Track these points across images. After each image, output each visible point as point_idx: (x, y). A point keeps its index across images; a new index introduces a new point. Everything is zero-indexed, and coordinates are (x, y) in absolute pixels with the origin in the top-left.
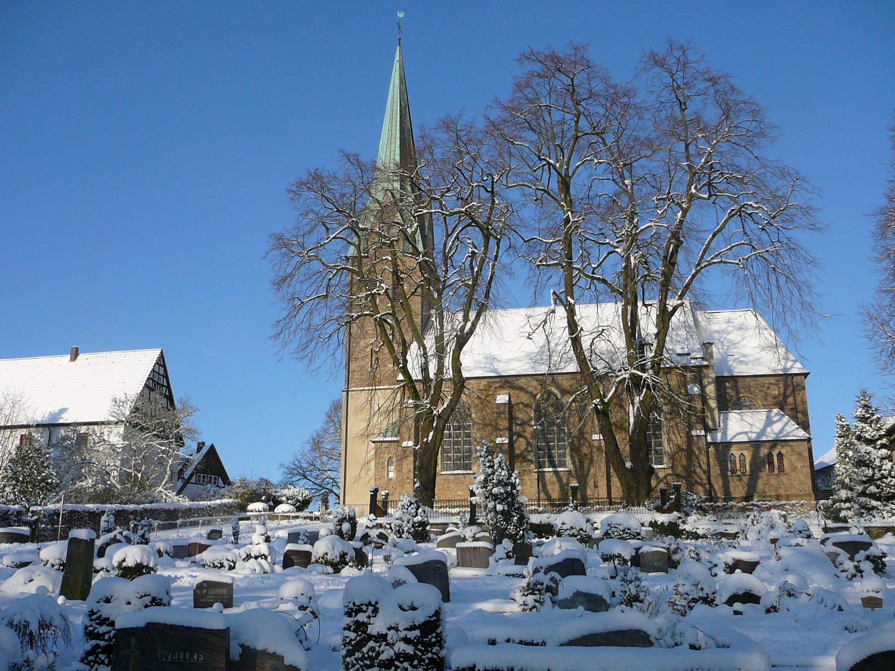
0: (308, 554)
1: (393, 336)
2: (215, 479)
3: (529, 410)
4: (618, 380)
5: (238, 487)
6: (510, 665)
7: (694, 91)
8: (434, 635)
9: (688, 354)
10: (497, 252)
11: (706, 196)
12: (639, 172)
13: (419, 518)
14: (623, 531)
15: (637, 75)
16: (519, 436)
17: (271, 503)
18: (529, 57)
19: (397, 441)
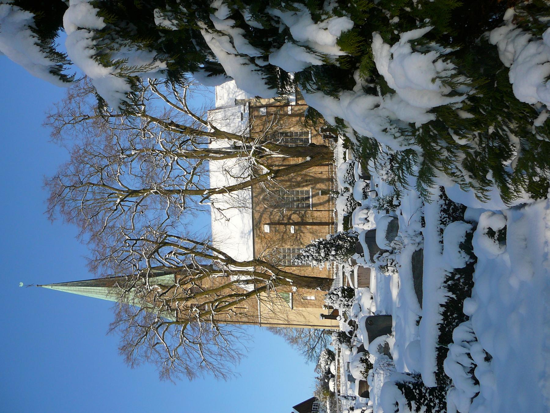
0: (361, 382)
1: (226, 301)
2: (314, 406)
3: (274, 213)
4: (256, 164)
5: (319, 396)
6: (434, 350)
7: (77, 110)
8: (414, 391)
9: (242, 113)
10: (175, 236)
11: (143, 107)
12: (127, 145)
13: (340, 293)
14: (348, 174)
15: (65, 146)
16: (290, 218)
17: (330, 375)
18: (50, 212)
19: (292, 294)
